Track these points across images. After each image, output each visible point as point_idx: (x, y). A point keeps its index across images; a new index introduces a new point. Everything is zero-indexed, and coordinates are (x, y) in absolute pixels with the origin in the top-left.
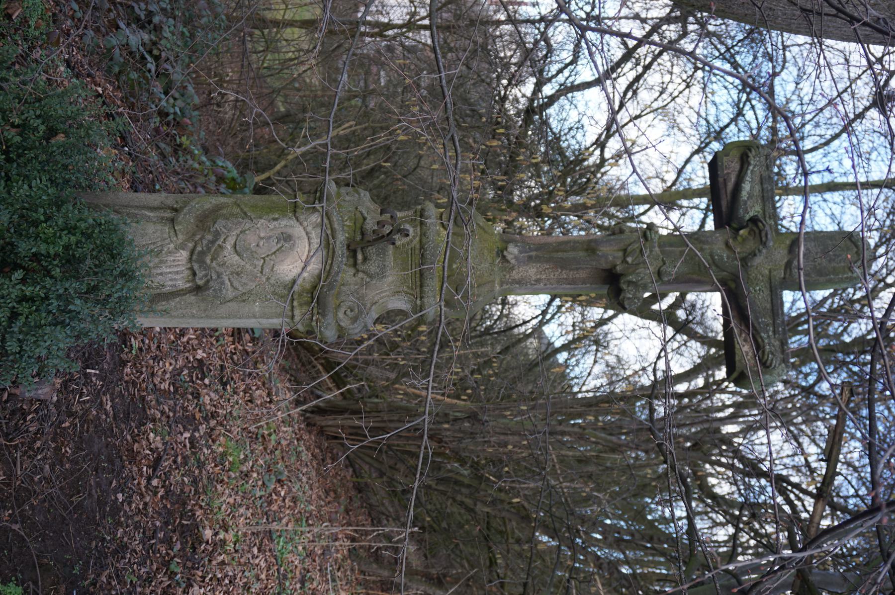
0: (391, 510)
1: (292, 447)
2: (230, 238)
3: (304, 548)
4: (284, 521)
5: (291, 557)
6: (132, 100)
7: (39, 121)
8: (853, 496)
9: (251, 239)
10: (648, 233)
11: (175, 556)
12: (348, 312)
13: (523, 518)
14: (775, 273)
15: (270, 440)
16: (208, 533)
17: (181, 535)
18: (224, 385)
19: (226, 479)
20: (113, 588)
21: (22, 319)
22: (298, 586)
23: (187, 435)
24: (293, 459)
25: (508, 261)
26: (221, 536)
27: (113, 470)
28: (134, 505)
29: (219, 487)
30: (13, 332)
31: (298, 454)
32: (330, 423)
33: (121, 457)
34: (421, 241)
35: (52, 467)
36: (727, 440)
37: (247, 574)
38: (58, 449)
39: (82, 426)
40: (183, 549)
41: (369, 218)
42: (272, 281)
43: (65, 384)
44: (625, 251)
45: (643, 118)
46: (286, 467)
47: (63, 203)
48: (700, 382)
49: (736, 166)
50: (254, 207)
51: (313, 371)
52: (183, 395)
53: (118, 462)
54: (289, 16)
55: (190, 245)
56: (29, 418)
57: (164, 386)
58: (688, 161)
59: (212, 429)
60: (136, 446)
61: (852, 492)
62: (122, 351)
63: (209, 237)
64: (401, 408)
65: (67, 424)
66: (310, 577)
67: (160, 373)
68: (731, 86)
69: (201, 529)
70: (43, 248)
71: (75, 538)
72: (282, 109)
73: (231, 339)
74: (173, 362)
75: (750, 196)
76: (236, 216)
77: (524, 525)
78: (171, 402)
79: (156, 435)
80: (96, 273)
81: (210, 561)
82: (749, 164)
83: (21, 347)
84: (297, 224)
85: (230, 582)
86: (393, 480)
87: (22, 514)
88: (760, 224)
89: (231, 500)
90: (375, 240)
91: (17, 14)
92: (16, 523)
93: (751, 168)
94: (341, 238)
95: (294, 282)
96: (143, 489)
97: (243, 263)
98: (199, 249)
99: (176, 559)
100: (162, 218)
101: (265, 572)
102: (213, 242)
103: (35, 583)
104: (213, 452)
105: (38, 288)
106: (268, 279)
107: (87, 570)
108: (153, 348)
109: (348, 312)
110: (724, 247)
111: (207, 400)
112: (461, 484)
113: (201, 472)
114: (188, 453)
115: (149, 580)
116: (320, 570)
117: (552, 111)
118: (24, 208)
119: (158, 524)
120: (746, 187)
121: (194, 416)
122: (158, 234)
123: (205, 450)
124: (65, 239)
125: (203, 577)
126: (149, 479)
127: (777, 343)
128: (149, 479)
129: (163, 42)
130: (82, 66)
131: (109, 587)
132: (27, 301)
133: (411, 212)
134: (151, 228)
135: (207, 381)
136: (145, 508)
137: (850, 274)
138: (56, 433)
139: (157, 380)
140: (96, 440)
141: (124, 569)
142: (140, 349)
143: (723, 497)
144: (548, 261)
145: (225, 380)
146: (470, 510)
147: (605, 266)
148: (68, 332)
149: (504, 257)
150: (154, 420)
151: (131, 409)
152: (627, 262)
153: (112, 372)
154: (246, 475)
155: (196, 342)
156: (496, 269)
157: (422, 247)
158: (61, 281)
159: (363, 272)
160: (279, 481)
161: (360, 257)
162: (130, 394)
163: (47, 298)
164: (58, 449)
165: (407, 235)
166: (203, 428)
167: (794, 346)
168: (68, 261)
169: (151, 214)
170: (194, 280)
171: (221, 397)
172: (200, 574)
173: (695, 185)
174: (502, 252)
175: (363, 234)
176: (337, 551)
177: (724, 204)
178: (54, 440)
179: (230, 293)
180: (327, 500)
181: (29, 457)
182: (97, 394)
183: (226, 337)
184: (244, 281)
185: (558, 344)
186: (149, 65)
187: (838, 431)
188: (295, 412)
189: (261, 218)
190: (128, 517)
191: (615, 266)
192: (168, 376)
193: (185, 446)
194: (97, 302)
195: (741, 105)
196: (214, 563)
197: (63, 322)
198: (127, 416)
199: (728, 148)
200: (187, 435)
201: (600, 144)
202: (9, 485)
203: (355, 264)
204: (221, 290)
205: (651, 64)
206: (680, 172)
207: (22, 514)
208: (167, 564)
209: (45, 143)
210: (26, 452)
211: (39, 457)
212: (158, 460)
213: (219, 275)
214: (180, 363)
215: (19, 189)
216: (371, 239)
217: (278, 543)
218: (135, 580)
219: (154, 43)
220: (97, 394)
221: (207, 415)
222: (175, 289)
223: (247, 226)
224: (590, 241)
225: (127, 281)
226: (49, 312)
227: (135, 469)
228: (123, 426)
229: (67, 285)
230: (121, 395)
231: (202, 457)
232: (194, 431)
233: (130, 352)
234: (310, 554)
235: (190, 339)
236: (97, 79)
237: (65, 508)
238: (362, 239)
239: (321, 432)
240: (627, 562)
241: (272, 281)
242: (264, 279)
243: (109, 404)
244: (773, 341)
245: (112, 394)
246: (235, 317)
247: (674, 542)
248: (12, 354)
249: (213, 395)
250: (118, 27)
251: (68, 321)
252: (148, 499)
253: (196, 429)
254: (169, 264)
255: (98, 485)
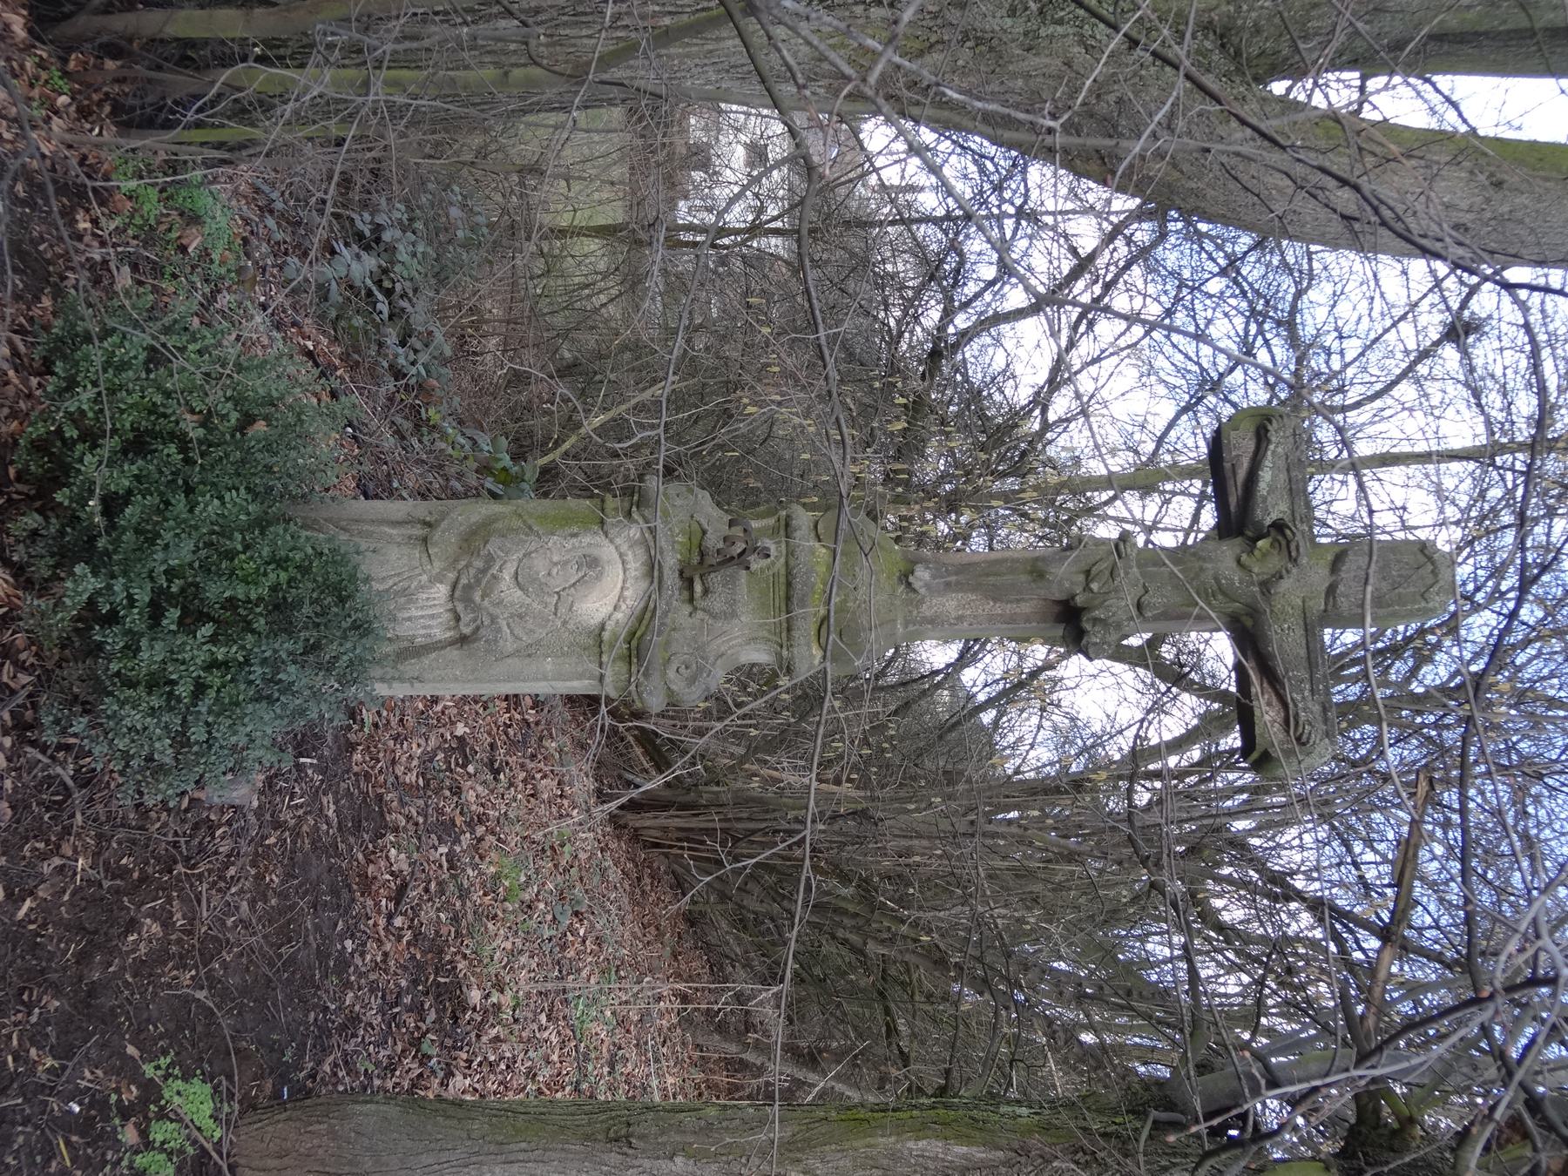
0: (738, 950)
1: (594, 862)
2: (509, 565)
3: (614, 1013)
4: (584, 973)
5: (594, 1027)
6: (356, 356)
7: (229, 405)
8: (1430, 927)
9: (540, 565)
10: (1122, 546)
11: (428, 1031)
12: (682, 670)
13: (935, 962)
14: (1311, 603)
15: (562, 853)
16: (475, 996)
17: (436, 999)
18: (496, 772)
19: (500, 914)
20: (339, 1081)
21: (212, 693)
22: (606, 1069)
23: (444, 850)
24: (596, 879)
25: (915, 591)
26: (494, 999)
27: (339, 906)
28: (368, 957)
29: (490, 925)
30: (199, 712)
31: (604, 871)
32: (648, 823)
33: (349, 886)
34: (787, 563)
35: (252, 904)
36: (1238, 844)
37: (530, 1054)
38: (259, 877)
39: (294, 842)
40: (439, 1020)
41: (710, 530)
42: (571, 626)
43: (270, 782)
44: (1088, 573)
45: (1103, 363)
46: (587, 891)
47: (269, 524)
48: (1195, 754)
49: (1249, 445)
50: (543, 518)
51: (621, 745)
52: (437, 792)
53: (345, 894)
54: (581, 219)
55: (452, 576)
56: (219, 833)
57: (411, 778)
58: (1171, 425)
59: (481, 840)
60: (371, 869)
61: (1428, 920)
62: (349, 728)
63: (479, 564)
64: (753, 800)
65: (272, 840)
66: (623, 1057)
67: (404, 759)
68: (1234, 312)
69: (464, 989)
70: (240, 591)
71: (285, 1008)
72: (567, 355)
73: (504, 704)
74: (422, 742)
75: (1272, 490)
76: (516, 531)
77: (937, 974)
78: (421, 802)
79: (399, 852)
80: (317, 625)
81: (478, 1036)
82: (1269, 442)
83: (209, 733)
84: (606, 542)
85: (508, 1067)
86: (744, 907)
87: (209, 976)
88: (1288, 532)
89: (508, 945)
90: (719, 564)
91: (194, 245)
92: (202, 988)
93: (1272, 447)
94: (671, 561)
95: (602, 627)
96: (382, 933)
97: (528, 601)
98: (464, 581)
99: (430, 1036)
100: (410, 537)
101: (557, 1051)
102: (484, 571)
103: (230, 1078)
104: (481, 874)
105: (234, 649)
106: (565, 623)
107: (302, 1057)
108: (394, 722)
109: (682, 670)
110: (1234, 565)
111: (471, 796)
112: (845, 912)
113: (463, 905)
114: (446, 876)
115: (391, 1068)
116: (637, 1045)
117: (970, 352)
118: (214, 532)
119: (404, 983)
120: (1266, 476)
121: (452, 820)
122: (405, 560)
123: (470, 872)
124: (272, 576)
125: (469, 1062)
126: (390, 917)
127: (1317, 708)
128: (390, 917)
129: (398, 268)
130: (284, 311)
131: (334, 1080)
132: (218, 668)
133: (771, 521)
134: (393, 553)
135: (471, 769)
136: (384, 961)
137: (1423, 604)
138: (256, 854)
139: (399, 770)
140: (314, 862)
141: (355, 1052)
142: (376, 725)
143: (1232, 928)
144: (974, 590)
145: (496, 765)
146: (855, 950)
147: (1058, 596)
148: (278, 711)
149: (909, 584)
150: (396, 830)
151: (363, 815)
152: (1091, 590)
153: (335, 761)
154: (529, 907)
155: (455, 711)
156: (898, 602)
157: (789, 573)
158: (267, 637)
159: (704, 610)
160: (576, 914)
161: (698, 588)
162: (361, 792)
163: (247, 662)
164: (259, 877)
165: (768, 556)
166: (466, 839)
167: (1337, 699)
168: (277, 607)
169: (394, 532)
170: (457, 627)
171: (492, 792)
172: (465, 1056)
173: (1183, 460)
174: (906, 577)
175: (702, 554)
176: (661, 1016)
177: (1233, 501)
178: (254, 864)
179: (509, 645)
180: (646, 940)
181: (220, 890)
182: (315, 795)
183: (497, 702)
184: (530, 626)
185: (982, 697)
186: (379, 306)
187: (1412, 842)
188: (601, 811)
189: (553, 534)
190: (361, 975)
191: (1073, 597)
192: (415, 762)
193: (441, 866)
194: (319, 666)
195: (1251, 339)
196: (484, 1039)
197: (268, 697)
198: (358, 826)
199: (1241, 414)
200: (444, 850)
201: (1041, 400)
202: (190, 933)
203: (691, 600)
204: (496, 641)
205: (1114, 281)
206: (1160, 441)
207: (209, 976)
208: (416, 1043)
209: (238, 435)
210: (215, 883)
211: (233, 890)
212: (402, 889)
213: (493, 619)
214: (433, 743)
215: (206, 505)
216: (714, 562)
217: (576, 1006)
218: (371, 1068)
219: (385, 271)
220: (315, 795)
221: (472, 819)
222: (429, 641)
223: (533, 546)
224: (1037, 559)
225: (362, 636)
226: (251, 683)
227: (370, 903)
228: (352, 840)
229: (277, 646)
230: (349, 794)
231: (465, 882)
232: (454, 843)
233: (361, 729)
234: (622, 1022)
235: (445, 707)
236: (306, 329)
237: (271, 965)
238: (701, 562)
239: (636, 836)
240: (1091, 1027)
241: (571, 626)
242: (559, 624)
243: (333, 807)
244: (1310, 705)
245: (336, 793)
246: (517, 679)
247: (1162, 995)
248: (197, 742)
249: (480, 789)
250: (333, 252)
251: (276, 695)
252: (388, 946)
253: (457, 841)
254: (420, 603)
255: (317, 928)
